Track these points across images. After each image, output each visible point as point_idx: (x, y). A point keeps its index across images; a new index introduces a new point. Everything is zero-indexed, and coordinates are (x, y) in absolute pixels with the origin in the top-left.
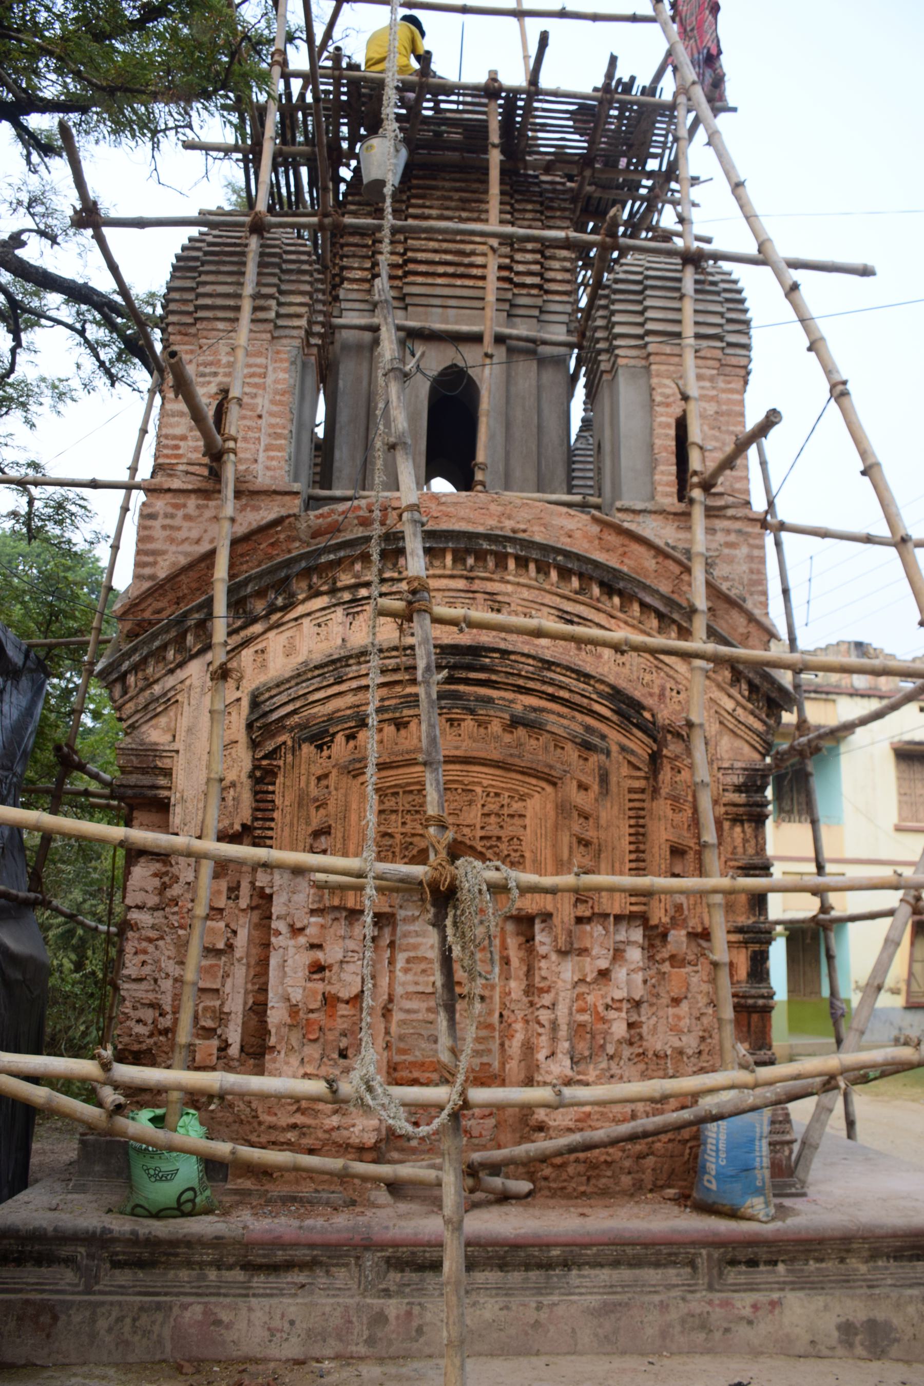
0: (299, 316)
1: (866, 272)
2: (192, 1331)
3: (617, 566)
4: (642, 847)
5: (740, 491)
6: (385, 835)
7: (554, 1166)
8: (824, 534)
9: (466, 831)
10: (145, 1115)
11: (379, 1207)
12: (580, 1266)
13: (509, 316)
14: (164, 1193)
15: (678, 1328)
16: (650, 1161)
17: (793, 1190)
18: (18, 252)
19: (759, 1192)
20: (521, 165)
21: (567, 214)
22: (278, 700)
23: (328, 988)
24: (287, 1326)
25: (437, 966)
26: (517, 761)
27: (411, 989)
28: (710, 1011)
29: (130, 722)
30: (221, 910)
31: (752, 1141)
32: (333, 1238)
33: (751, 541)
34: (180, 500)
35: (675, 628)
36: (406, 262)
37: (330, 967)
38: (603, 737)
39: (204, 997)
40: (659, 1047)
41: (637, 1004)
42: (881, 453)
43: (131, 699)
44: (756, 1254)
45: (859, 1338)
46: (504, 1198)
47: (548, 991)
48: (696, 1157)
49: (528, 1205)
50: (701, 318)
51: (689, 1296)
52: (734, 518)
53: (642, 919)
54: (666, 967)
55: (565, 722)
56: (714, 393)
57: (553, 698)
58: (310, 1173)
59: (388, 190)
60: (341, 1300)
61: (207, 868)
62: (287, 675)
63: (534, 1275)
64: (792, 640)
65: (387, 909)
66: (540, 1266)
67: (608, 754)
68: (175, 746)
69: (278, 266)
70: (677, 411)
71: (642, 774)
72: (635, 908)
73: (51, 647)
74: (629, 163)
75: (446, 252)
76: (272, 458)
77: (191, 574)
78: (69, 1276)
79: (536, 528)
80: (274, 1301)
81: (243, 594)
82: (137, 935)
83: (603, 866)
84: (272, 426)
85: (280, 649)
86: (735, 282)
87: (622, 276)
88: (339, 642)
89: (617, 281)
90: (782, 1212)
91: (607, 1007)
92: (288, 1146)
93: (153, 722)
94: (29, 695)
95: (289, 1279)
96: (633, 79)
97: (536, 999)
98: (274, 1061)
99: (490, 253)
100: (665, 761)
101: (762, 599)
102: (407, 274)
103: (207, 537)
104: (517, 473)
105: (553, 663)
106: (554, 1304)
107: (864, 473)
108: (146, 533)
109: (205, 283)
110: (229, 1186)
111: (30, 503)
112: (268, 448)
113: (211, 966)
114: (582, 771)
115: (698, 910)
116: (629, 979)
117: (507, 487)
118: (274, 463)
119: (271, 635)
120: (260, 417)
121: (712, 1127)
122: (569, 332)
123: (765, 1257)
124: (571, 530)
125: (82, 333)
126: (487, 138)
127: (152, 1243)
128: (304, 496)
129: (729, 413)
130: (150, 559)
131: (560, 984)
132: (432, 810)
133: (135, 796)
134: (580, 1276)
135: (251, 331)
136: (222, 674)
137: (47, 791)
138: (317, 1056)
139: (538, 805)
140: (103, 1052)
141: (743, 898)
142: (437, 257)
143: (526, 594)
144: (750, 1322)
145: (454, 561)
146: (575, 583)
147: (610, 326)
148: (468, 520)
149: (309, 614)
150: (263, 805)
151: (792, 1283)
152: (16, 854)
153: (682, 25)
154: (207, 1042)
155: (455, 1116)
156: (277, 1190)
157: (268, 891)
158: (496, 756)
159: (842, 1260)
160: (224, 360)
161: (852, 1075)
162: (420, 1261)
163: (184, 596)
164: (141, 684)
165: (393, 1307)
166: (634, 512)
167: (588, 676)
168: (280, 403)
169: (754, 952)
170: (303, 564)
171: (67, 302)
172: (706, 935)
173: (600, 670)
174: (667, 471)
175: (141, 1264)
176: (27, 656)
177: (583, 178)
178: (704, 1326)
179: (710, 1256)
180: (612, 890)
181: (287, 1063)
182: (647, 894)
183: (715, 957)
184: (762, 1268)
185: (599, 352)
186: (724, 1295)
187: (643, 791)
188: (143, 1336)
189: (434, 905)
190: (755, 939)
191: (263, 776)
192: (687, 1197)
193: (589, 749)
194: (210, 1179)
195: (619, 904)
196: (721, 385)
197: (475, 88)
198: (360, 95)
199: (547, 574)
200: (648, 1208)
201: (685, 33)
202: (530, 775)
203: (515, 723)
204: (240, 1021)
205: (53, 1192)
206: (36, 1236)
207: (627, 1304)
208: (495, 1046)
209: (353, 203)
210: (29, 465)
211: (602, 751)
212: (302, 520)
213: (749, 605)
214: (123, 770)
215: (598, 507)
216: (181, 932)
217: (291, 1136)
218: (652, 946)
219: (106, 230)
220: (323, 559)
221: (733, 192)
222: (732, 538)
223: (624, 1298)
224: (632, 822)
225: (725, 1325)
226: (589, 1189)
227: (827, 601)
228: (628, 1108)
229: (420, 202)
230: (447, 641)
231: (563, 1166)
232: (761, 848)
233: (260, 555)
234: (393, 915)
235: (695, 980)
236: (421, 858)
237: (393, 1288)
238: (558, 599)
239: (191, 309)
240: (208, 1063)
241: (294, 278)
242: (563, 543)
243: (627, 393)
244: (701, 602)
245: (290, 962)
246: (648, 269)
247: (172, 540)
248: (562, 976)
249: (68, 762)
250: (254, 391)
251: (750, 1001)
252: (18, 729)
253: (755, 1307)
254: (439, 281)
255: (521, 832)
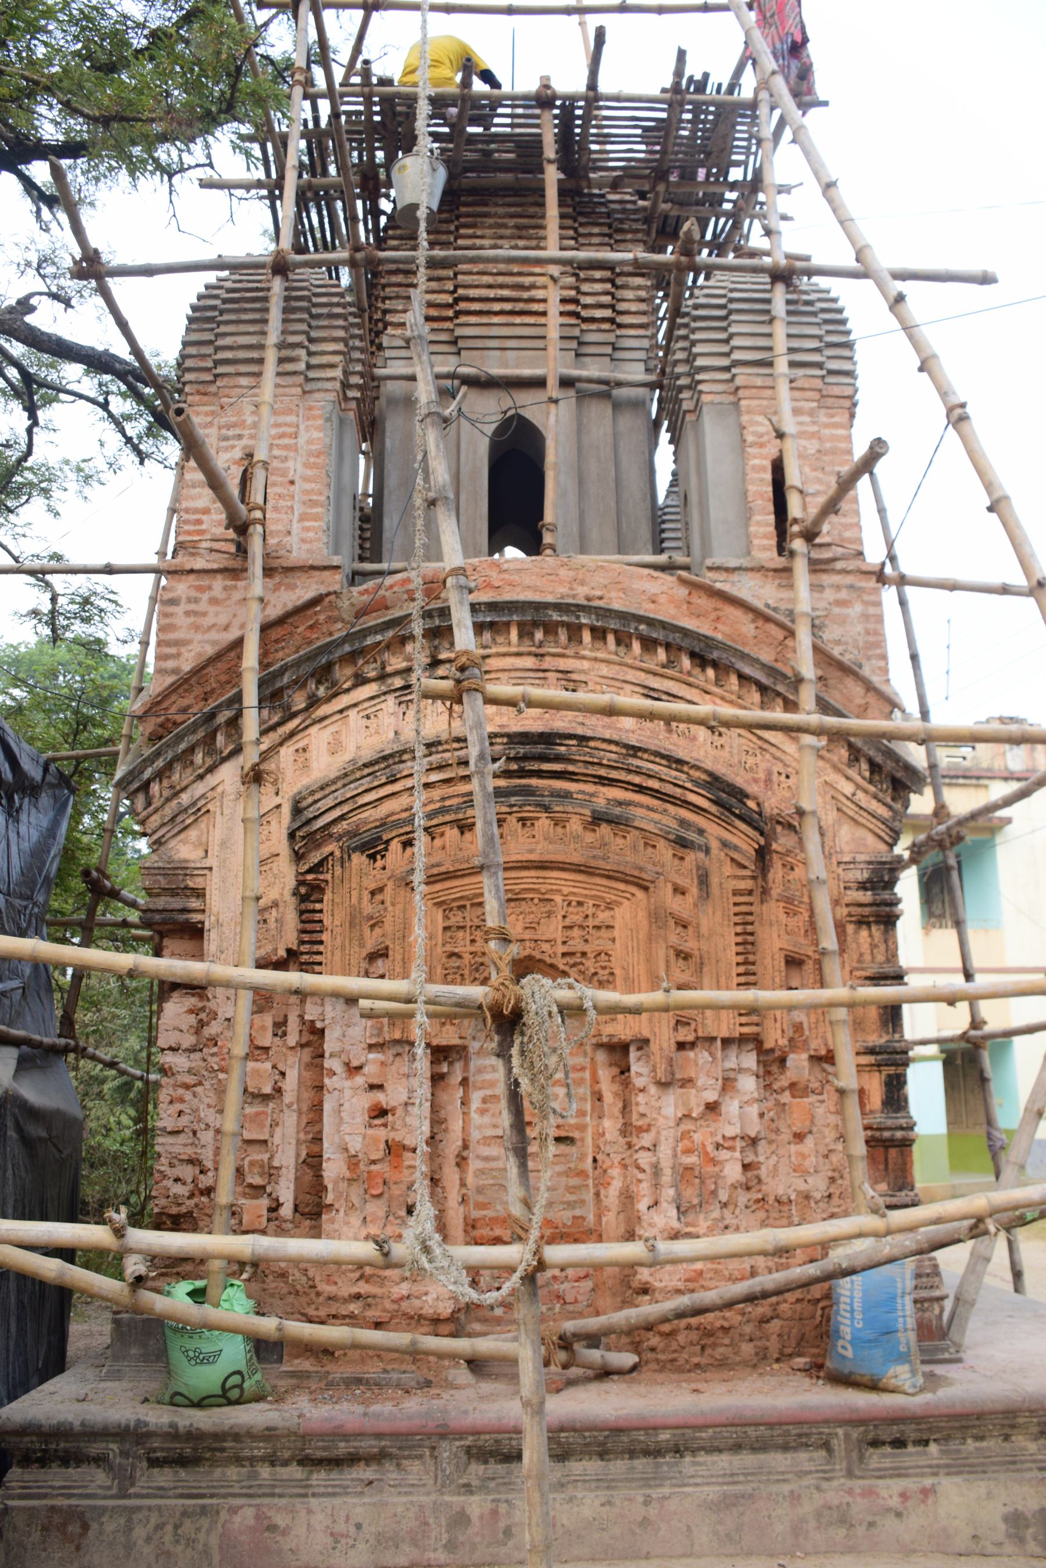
0: (332, 366)
1: (986, 279)
2: (243, 1538)
3: (709, 633)
4: (751, 958)
5: (850, 541)
6: (452, 955)
7: (662, 1334)
8: (952, 586)
9: (546, 947)
10: (183, 1288)
11: (457, 1388)
12: (694, 1452)
13: (577, 355)
14: (205, 1378)
15: (813, 1524)
16: (775, 1325)
17: (947, 1356)
18: (29, 319)
19: (904, 1358)
20: (584, 184)
21: (640, 236)
22: (323, 805)
23: (392, 1135)
24: (352, 1530)
25: (503, 1104)
26: (601, 864)
27: (490, 1132)
28: (840, 1147)
29: (155, 837)
30: (266, 1049)
31: (893, 1298)
32: (403, 1425)
33: (866, 598)
34: (205, 581)
35: (780, 701)
36: (456, 301)
37: (393, 1110)
38: (701, 832)
39: (250, 1149)
40: (780, 1191)
41: (754, 1142)
42: (1008, 484)
43: (156, 811)
44: (903, 1432)
45: (1031, 1530)
46: (605, 1373)
47: (648, 1130)
48: (828, 1320)
49: (633, 1381)
50: (795, 344)
51: (825, 1485)
52: (845, 572)
53: (756, 1041)
54: (786, 1097)
55: (656, 816)
56: (815, 428)
57: (641, 789)
58: (378, 1352)
59: (422, 214)
60: (414, 1499)
61: (246, 999)
62: (332, 776)
63: (640, 1463)
64: (925, 714)
65: (457, 1041)
66: (647, 1453)
67: (707, 851)
68: (207, 863)
69: (307, 310)
70: (772, 452)
71: (748, 873)
72: (746, 1030)
73: (79, 760)
74: (708, 175)
75: (501, 286)
76: (307, 529)
77: (219, 665)
78: (100, 1477)
79: (613, 594)
80: (337, 1501)
81: (278, 685)
82: (171, 1081)
83: (706, 980)
84: (307, 492)
85: (324, 747)
86: (835, 300)
87: (702, 301)
88: (392, 735)
89: (696, 307)
90: (932, 1381)
91: (718, 1146)
92: (351, 1320)
93: (182, 836)
94: (51, 814)
95: (354, 1475)
96: (706, 76)
97: (635, 1140)
98: (332, 1221)
99: (550, 284)
100: (775, 856)
101: (882, 663)
102: (458, 314)
103: (236, 623)
104: (594, 535)
105: (640, 749)
106: (665, 1498)
107: (990, 509)
108: (167, 621)
109: (225, 335)
110: (285, 1368)
111: (54, 600)
112: (301, 519)
113: (257, 1114)
114: (677, 872)
115: (821, 1030)
116: (742, 1112)
117: (583, 551)
118: (311, 534)
119: (313, 730)
120: (292, 482)
121: (845, 1282)
122: (648, 370)
123: (913, 1436)
124: (656, 595)
125: (105, 406)
126: (541, 153)
127: (194, 1436)
128: (348, 570)
129: (833, 452)
130: (173, 650)
131: (661, 1121)
132: (492, 922)
133: (164, 922)
134: (695, 1464)
135: (277, 386)
136: (255, 777)
137: (80, 924)
138: (381, 1214)
139: (629, 913)
140: (115, 1216)
141: (873, 1013)
142: (491, 293)
143: (604, 669)
144: (899, 1515)
145: (521, 636)
146: (662, 654)
147: (690, 360)
148: (535, 589)
149: (355, 705)
150: (310, 925)
151: (947, 1466)
152: (43, 994)
153: (761, 12)
154: (255, 1202)
155: (530, 1279)
156: (339, 1371)
157: (319, 1025)
158: (576, 858)
159: (1007, 1438)
160: (250, 420)
161: (1006, 1216)
162: (499, 1451)
163: (213, 691)
164: (167, 793)
165: (476, 1505)
166: (727, 570)
167: (680, 762)
168: (315, 466)
169: (889, 1076)
170: (347, 648)
171: (87, 373)
172: (829, 1058)
173: (694, 755)
174: (765, 520)
175: (182, 1462)
176: (46, 770)
177: (657, 194)
178: (844, 1520)
179: (847, 1436)
180: (718, 1007)
181: (347, 1223)
182: (752, 1010)
183: (841, 1084)
184: (911, 1449)
185: (680, 389)
186: (866, 1482)
187: (750, 893)
188: (187, 1545)
189: (498, 1033)
190: (891, 1062)
191: (309, 893)
192: (820, 1367)
193: (685, 847)
194: (260, 1359)
195: (726, 1026)
196: (824, 420)
197: (525, 97)
198: (395, 114)
199: (629, 646)
200: (773, 1381)
201: (764, 21)
202: (617, 879)
203: (598, 819)
204: (292, 1176)
205: (84, 1380)
206: (61, 1432)
207: (751, 1496)
208: (589, 1196)
209: (393, 238)
210: (51, 558)
211: (700, 848)
212: (344, 597)
213: (866, 672)
214: (149, 892)
215: (687, 568)
216: (221, 1076)
217: (354, 1307)
218: (768, 1073)
219: (112, 283)
220: (369, 641)
221: (824, 194)
222: (843, 595)
223: (747, 1488)
224: (739, 929)
225: (870, 1518)
226: (704, 1361)
227: (960, 666)
228: (746, 1264)
229: (470, 231)
230: (515, 727)
231: (672, 1334)
232: (892, 955)
233: (298, 639)
234: (465, 1048)
235: (820, 1111)
236: (479, 974)
237: (475, 1483)
238: (643, 675)
239: (210, 364)
240: (257, 1226)
241: (325, 323)
242: (646, 610)
243: (713, 433)
244: (808, 669)
245: (346, 1106)
246: (732, 290)
247: (197, 628)
248: (663, 1111)
249: (100, 889)
250: (284, 453)
251: (887, 1134)
252: (39, 853)
253: (904, 1496)
254: (496, 320)
255: (608, 946)
